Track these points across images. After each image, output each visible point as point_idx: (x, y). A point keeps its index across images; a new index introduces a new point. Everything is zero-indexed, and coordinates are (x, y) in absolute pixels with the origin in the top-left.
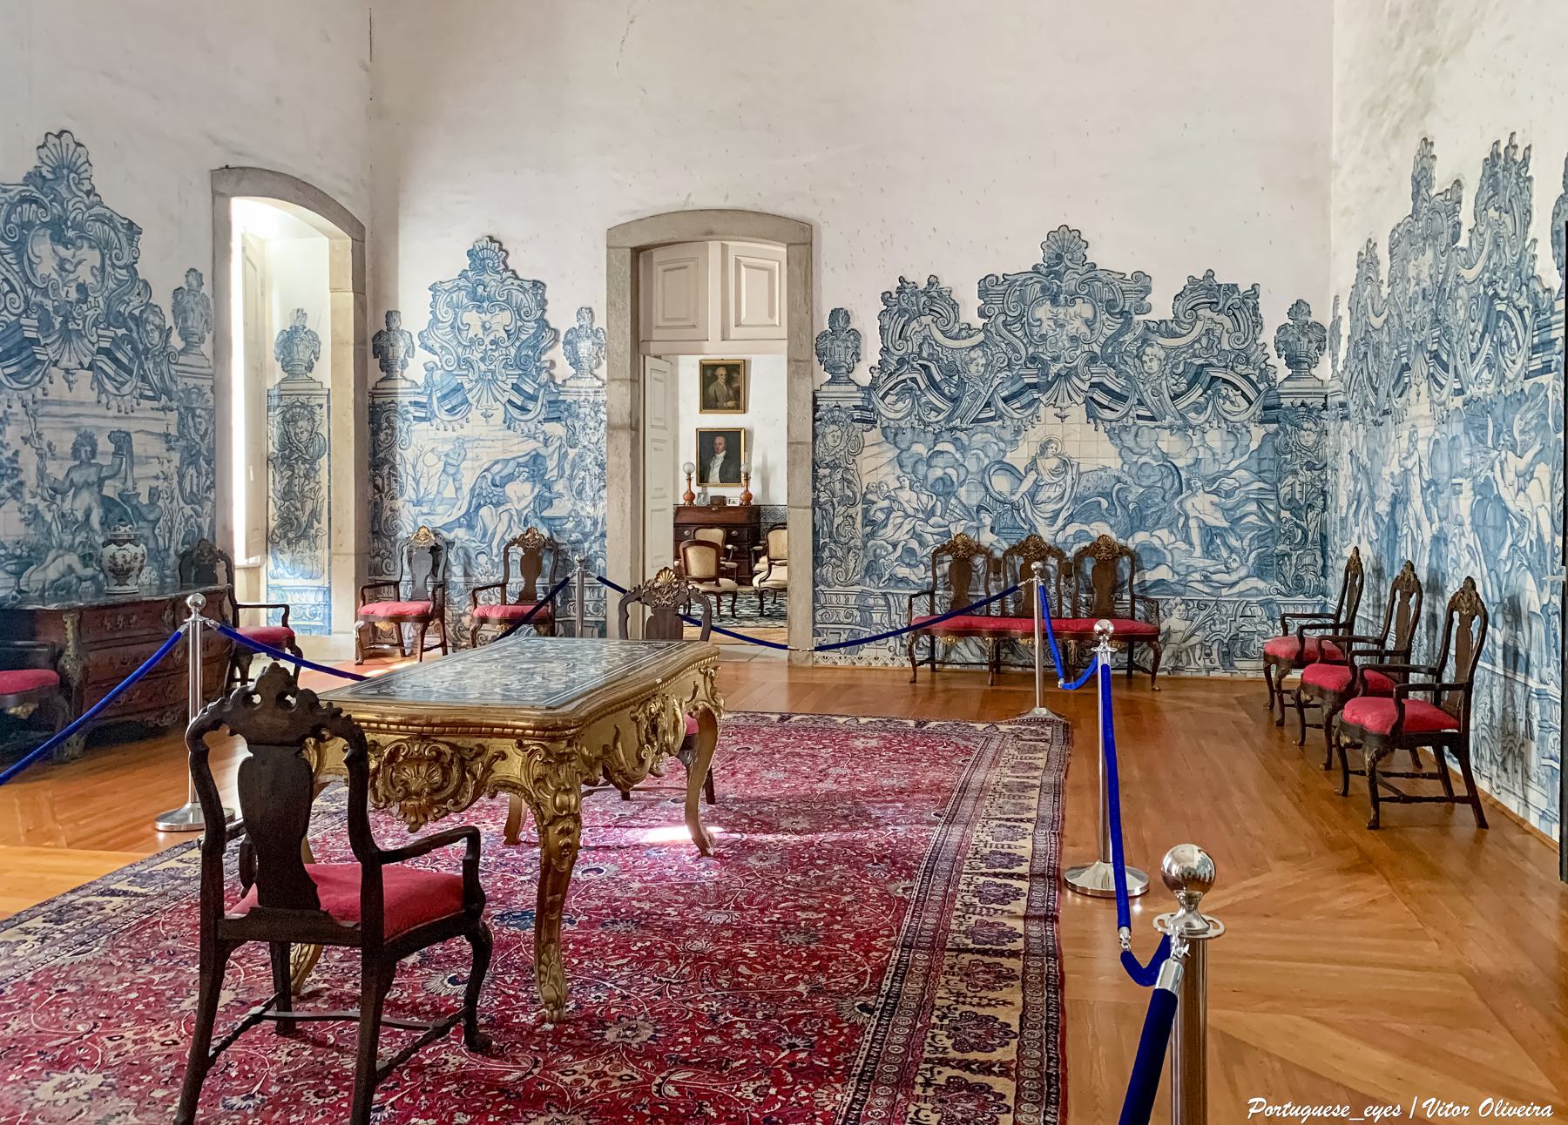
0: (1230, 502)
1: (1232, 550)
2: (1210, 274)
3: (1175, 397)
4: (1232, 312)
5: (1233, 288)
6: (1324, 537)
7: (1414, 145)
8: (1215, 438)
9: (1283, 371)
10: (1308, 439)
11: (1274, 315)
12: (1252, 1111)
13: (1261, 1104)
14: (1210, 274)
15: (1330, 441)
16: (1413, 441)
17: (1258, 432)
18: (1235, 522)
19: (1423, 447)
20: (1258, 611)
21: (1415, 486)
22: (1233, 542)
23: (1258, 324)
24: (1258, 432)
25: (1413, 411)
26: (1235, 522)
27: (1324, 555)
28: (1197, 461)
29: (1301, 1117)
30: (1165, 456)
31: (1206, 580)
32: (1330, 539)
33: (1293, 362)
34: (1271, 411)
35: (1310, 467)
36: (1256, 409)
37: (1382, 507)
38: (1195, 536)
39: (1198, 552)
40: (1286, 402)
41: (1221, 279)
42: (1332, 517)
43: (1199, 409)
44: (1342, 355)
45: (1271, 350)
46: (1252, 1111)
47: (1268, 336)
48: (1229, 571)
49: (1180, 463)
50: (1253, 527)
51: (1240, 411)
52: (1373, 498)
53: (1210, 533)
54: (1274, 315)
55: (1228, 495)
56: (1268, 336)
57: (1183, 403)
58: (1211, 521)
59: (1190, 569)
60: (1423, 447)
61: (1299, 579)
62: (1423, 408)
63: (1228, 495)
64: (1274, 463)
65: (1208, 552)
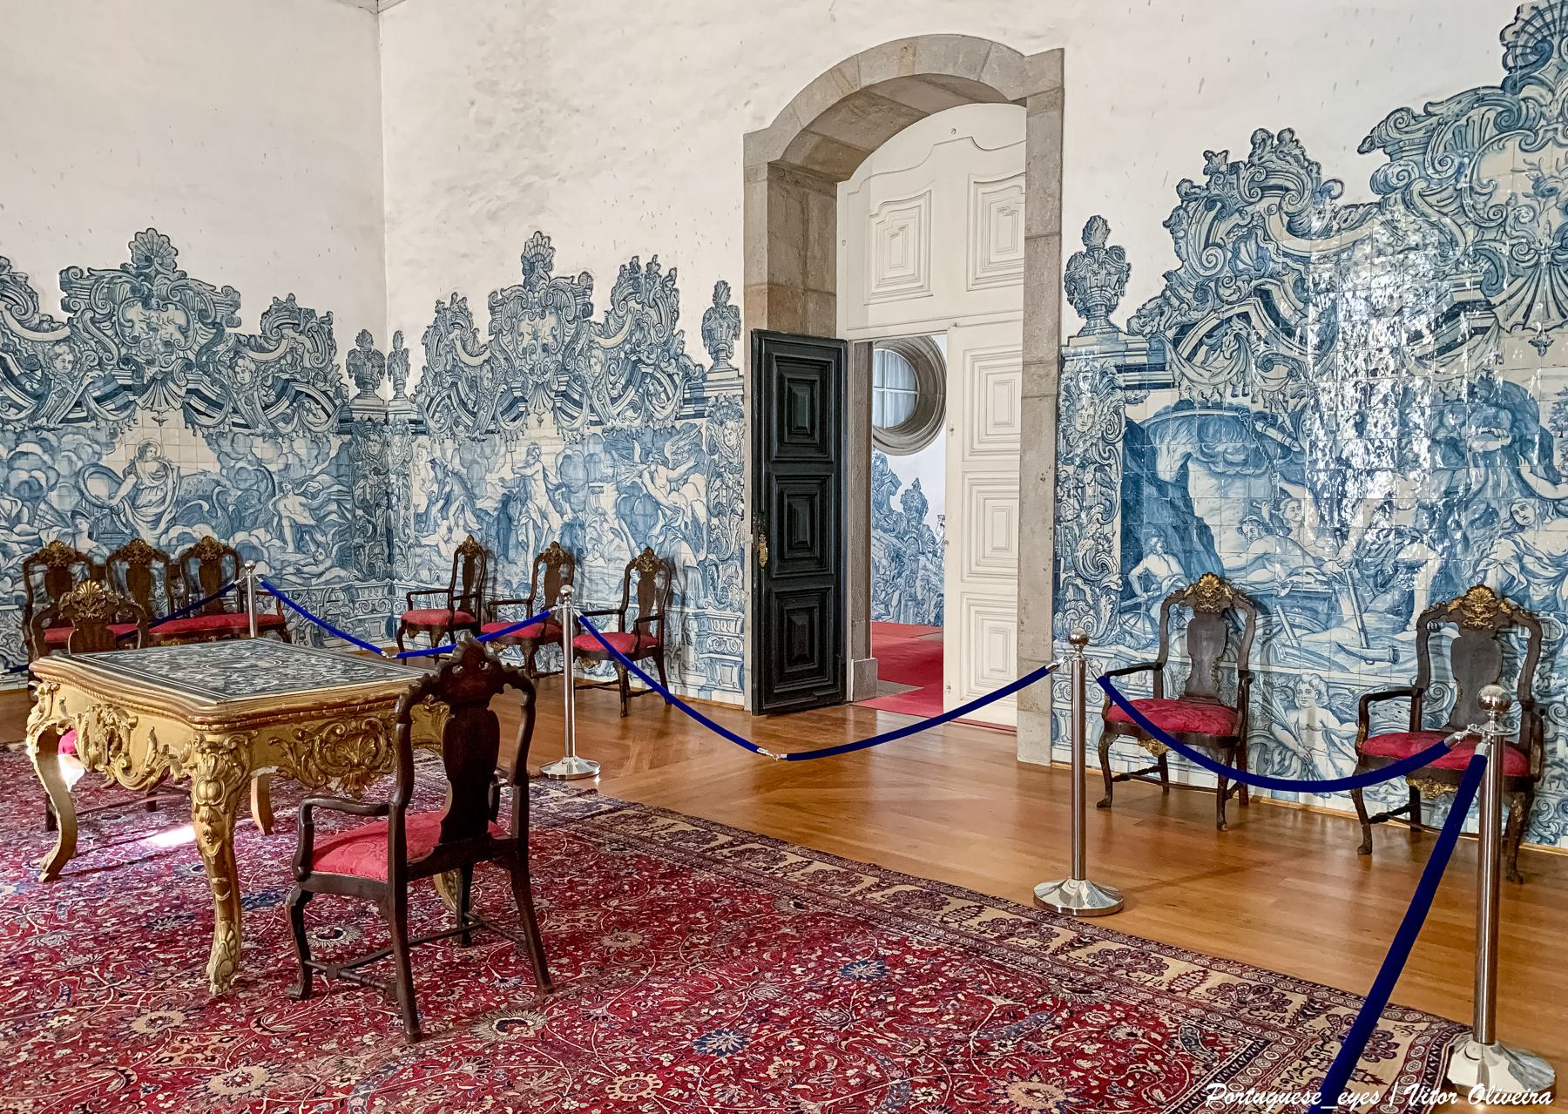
1: (318, 545)
3: (266, 407)
6: (389, 531)
8: (301, 446)
9: (353, 391)
10: (375, 449)
11: (345, 342)
17: (336, 442)
18: (320, 520)
19: (547, 460)
20: (341, 596)
22: (319, 537)
24: (336, 442)
25: (533, 432)
26: (320, 520)
27: (390, 544)
28: (287, 466)
30: (260, 462)
31: (299, 572)
33: (361, 383)
34: (346, 424)
35: (377, 472)
39: (291, 548)
40: (357, 416)
42: (399, 515)
43: (287, 419)
45: (343, 370)
47: (341, 359)
48: (317, 563)
49: (272, 468)
50: (334, 523)
51: (321, 422)
52: (471, 496)
53: (300, 530)
54: (345, 342)
55: (314, 497)
56: (341, 359)
57: (273, 413)
61: (371, 566)
62: (549, 428)
64: (349, 468)
65: (298, 549)
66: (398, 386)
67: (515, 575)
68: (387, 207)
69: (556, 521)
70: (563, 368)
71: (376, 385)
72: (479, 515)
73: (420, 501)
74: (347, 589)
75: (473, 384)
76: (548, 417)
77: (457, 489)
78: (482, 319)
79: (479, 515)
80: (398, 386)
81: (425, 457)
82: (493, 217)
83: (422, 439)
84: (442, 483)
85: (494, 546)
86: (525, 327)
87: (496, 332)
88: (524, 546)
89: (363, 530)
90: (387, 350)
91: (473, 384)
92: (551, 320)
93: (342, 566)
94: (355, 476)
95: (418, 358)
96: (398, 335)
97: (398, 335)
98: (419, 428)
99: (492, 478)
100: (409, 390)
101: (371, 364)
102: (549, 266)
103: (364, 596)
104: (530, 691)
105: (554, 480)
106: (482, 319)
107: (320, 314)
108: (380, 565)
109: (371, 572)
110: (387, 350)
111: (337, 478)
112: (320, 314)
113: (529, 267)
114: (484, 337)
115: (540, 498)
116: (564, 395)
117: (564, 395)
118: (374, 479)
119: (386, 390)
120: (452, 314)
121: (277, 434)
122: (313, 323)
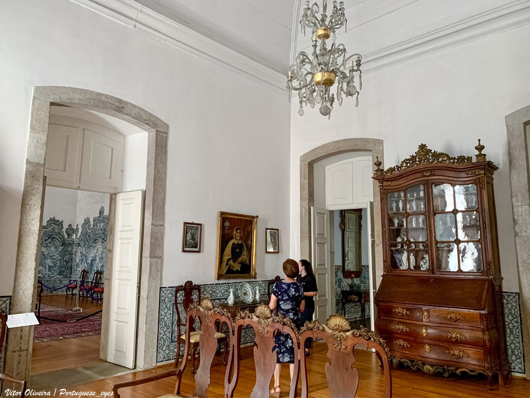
0: (54, 261)
1: (54, 270)
2: (54, 218)
3: (46, 240)
4: (58, 225)
5: (58, 221)
6: (71, 267)
7: (371, 149)
8: (52, 249)
9: (66, 237)
10: (70, 249)
11: (65, 226)
12: (61, 393)
13: (64, 391)
14: (54, 218)
15: (74, 250)
16: (97, 251)
17: (61, 248)
18: (55, 265)
19: (100, 252)
20: (58, 282)
21: (98, 258)
22: (54, 269)
23: (62, 228)
24: (61, 248)
25: (98, 247)
26: (55, 265)
27: (71, 270)
28: (49, 253)
29: (78, 396)
30: (43, 252)
31: (49, 276)
32: (73, 268)
33: (68, 235)
34: (63, 244)
35: (70, 254)
36: (61, 243)
37: (89, 261)
38: (47, 268)
39: (47, 271)
40: (66, 242)
41: (56, 219)
42: (74, 264)
43: (50, 243)
44: (79, 235)
45: (64, 233)
46: (61, 393)
47: (64, 230)
48: (53, 274)
49: (45, 253)
50: (58, 266)
51: (57, 243)
52: (86, 260)
53: (50, 267)
54: (65, 226)
55: (54, 259)
56: (64, 230)
57: (47, 242)
58: (51, 265)
59: (46, 274)
60: (100, 252)
61: (66, 275)
62: (100, 246)
63: (54, 259)
64: (63, 254)
65: (49, 271)
66: (76, 236)
67: (91, 277)
68: (78, 198)
69: (100, 265)
70: (104, 234)
71: (72, 235)
72: (87, 263)
73: (78, 261)
74: (59, 280)
75: (89, 236)
76: (100, 243)
77: (84, 258)
78: (92, 223)
79: (87, 263)
80: (76, 236)
81: (79, 251)
82: (96, 203)
83: (79, 247)
84: (82, 257)
85: (89, 271)
86: (98, 225)
87: (94, 226)
88: (94, 270)
89: (65, 267)
90: (75, 228)
91: (89, 236)
92: (103, 224)
93: (60, 275)
94: (65, 255)
95: (80, 230)
96: (77, 225)
97: (77, 225)
98: (79, 245)
99: (90, 256)
100: (78, 237)
101: (71, 231)
102: (103, 213)
103: (64, 282)
104: (199, 291)
105: (100, 256)
106: (92, 223)
107: (60, 221)
108: (68, 275)
109: (66, 277)
110: (75, 228)
111: (60, 256)
112: (60, 221)
113: (100, 214)
114: (92, 226)
115: (98, 261)
116: (103, 239)
117: (103, 239)
118: (69, 256)
119: (74, 236)
120: (87, 221)
121: (48, 246)
122: (59, 223)
